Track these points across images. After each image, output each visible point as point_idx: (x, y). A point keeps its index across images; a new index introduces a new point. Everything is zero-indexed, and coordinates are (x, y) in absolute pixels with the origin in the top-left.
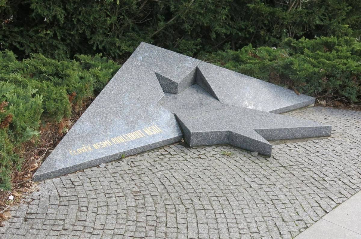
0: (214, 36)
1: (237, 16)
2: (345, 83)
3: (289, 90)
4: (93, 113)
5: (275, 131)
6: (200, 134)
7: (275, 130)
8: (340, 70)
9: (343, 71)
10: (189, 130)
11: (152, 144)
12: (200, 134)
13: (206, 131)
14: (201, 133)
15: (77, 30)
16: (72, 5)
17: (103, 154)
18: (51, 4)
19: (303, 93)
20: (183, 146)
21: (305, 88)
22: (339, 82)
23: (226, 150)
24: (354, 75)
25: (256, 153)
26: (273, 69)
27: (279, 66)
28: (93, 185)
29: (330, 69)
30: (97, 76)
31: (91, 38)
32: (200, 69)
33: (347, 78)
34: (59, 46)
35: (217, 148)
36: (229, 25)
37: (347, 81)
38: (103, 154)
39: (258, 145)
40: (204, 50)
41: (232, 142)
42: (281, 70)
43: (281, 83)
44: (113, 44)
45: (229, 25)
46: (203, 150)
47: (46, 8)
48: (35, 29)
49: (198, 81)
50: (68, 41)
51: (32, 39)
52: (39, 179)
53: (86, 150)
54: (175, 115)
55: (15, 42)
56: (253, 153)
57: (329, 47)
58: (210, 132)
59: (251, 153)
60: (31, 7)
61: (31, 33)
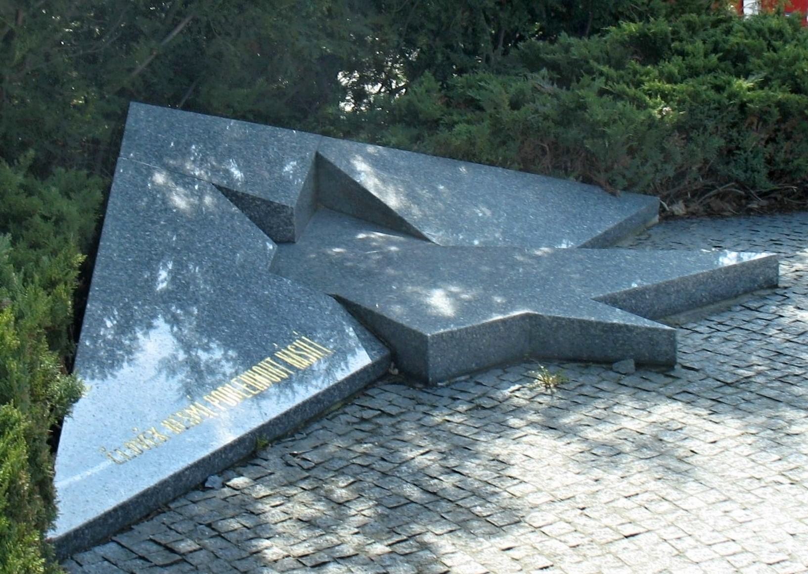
3: (586, 187)
5: (644, 294)
6: (452, 337)
8: (712, 106)
10: (414, 331)
12: (452, 337)
13: (468, 325)
14: (456, 332)
19: (625, 189)
20: (405, 387)
21: (629, 175)
22: (718, 142)
25: (630, 365)
26: (527, 130)
27: (546, 118)
28: (234, 541)
33: (734, 125)
35: (506, 373)
39: (629, 337)
42: (553, 131)
43: (555, 167)
46: (472, 384)
54: (339, 299)
56: (621, 366)
58: (479, 326)
59: (615, 365)
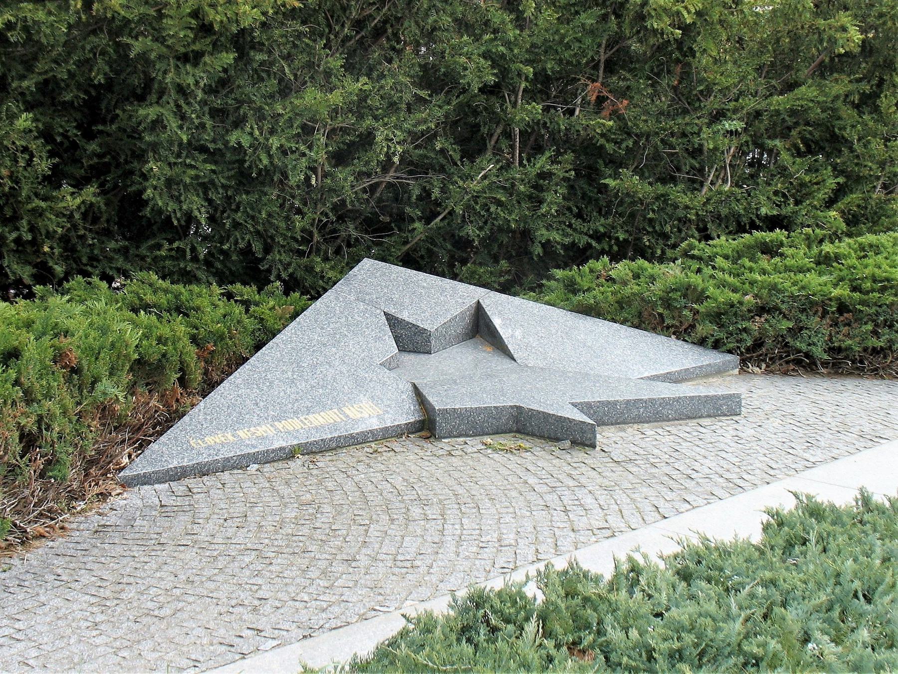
0: (538, 250)
1: (589, 209)
2: (801, 321)
4: (244, 380)
7: (615, 403)
9: (792, 297)
11: (357, 434)
15: (236, 243)
16: (221, 191)
17: (254, 446)
18: (182, 191)
23: (507, 441)
24: (817, 303)
25: (568, 443)
29: (765, 292)
30: (262, 319)
31: (263, 259)
32: (484, 306)
34: (199, 274)
36: (570, 226)
37: (804, 318)
38: (255, 447)
40: (521, 285)
41: (527, 426)
44: (309, 269)
45: (570, 226)
47: (172, 197)
48: (151, 242)
49: (480, 328)
50: (219, 265)
51: (146, 261)
52: (126, 484)
53: (223, 439)
55: (111, 268)
57: (769, 250)
60: (145, 197)
61: (143, 251)
